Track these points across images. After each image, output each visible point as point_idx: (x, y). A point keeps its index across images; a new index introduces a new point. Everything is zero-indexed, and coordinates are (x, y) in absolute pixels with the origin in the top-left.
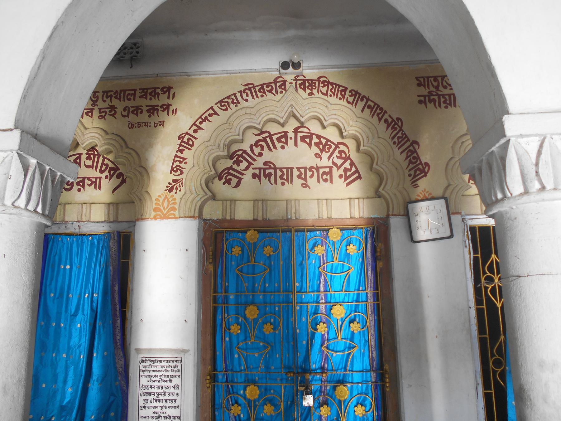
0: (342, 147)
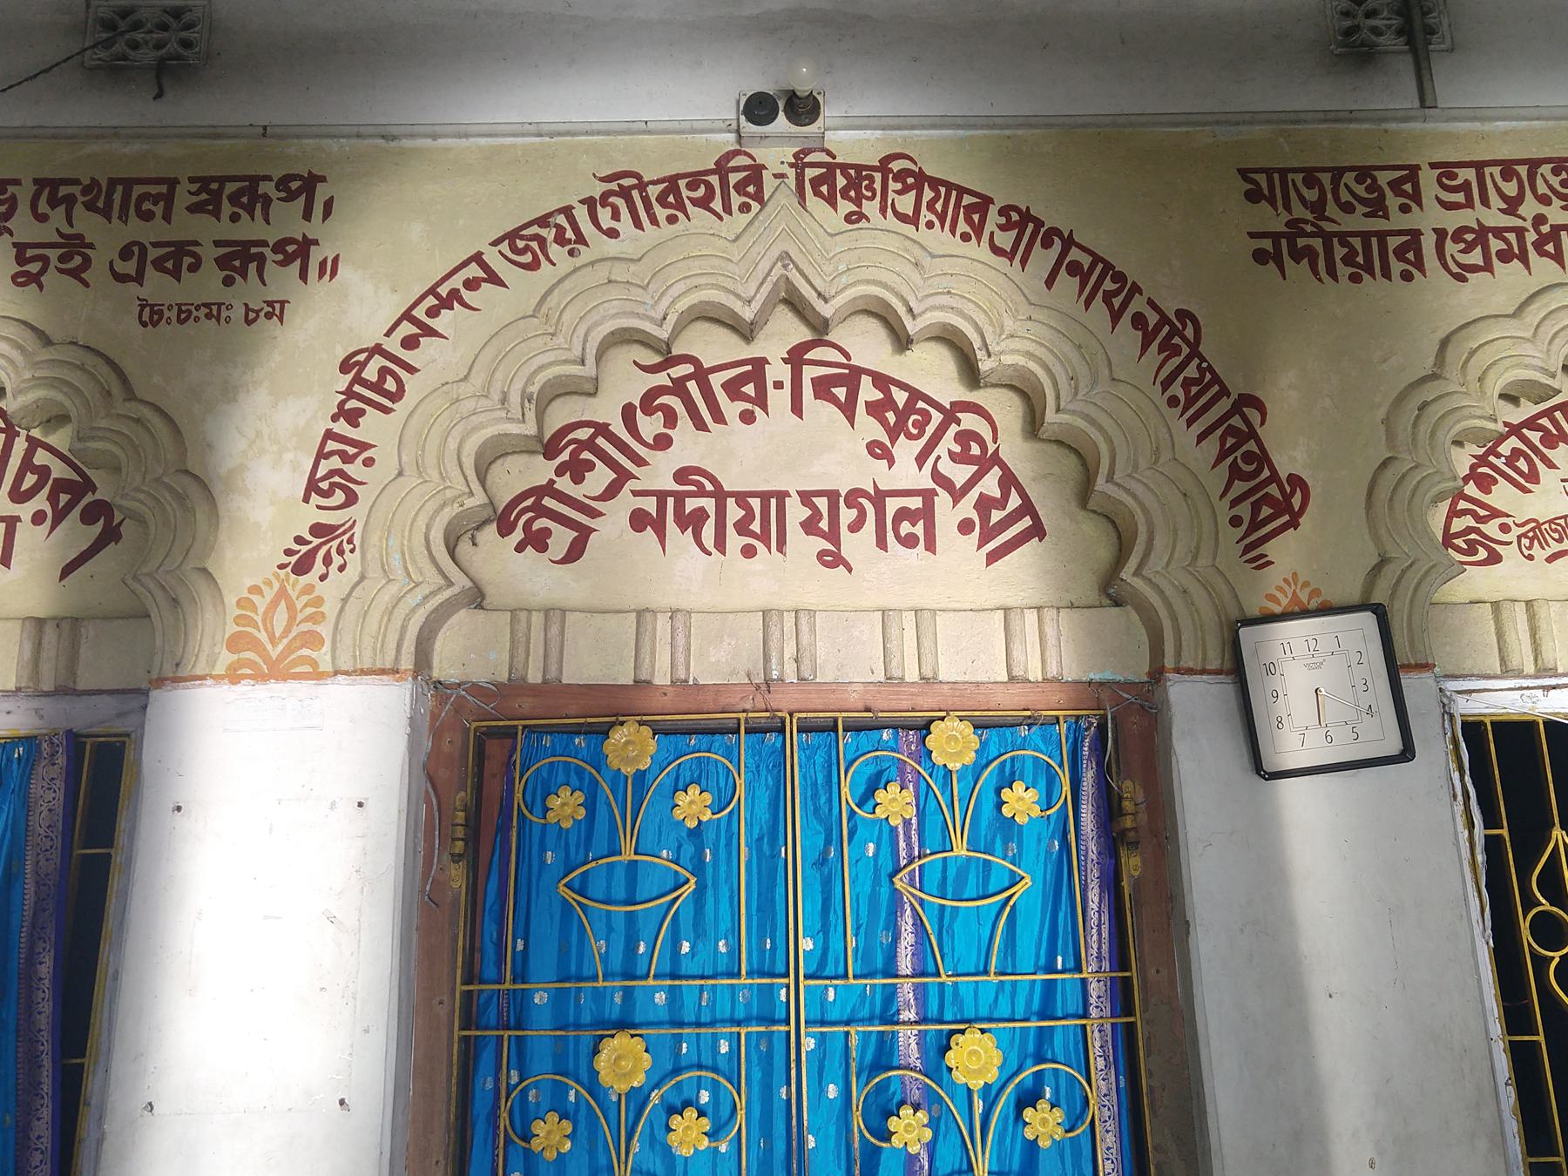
0: (969, 421)
